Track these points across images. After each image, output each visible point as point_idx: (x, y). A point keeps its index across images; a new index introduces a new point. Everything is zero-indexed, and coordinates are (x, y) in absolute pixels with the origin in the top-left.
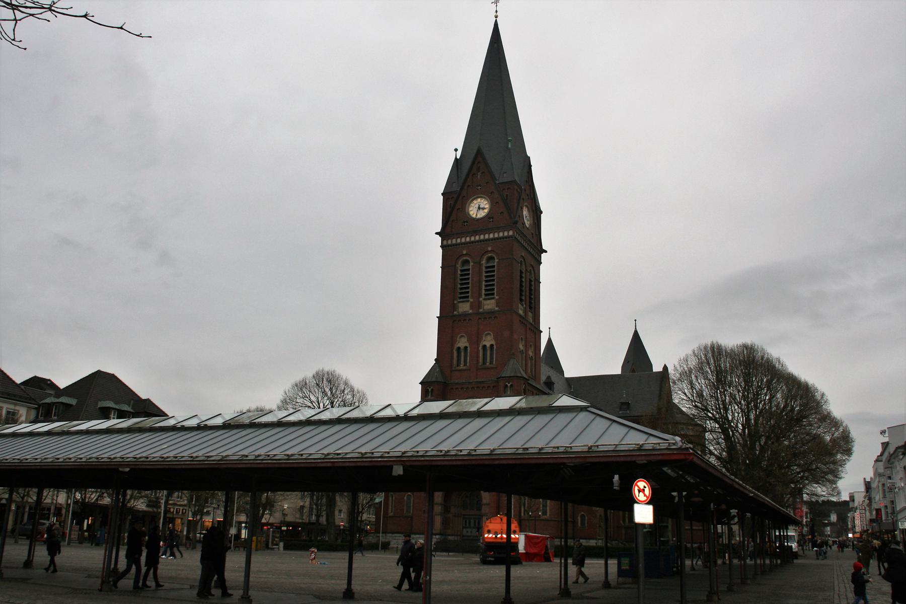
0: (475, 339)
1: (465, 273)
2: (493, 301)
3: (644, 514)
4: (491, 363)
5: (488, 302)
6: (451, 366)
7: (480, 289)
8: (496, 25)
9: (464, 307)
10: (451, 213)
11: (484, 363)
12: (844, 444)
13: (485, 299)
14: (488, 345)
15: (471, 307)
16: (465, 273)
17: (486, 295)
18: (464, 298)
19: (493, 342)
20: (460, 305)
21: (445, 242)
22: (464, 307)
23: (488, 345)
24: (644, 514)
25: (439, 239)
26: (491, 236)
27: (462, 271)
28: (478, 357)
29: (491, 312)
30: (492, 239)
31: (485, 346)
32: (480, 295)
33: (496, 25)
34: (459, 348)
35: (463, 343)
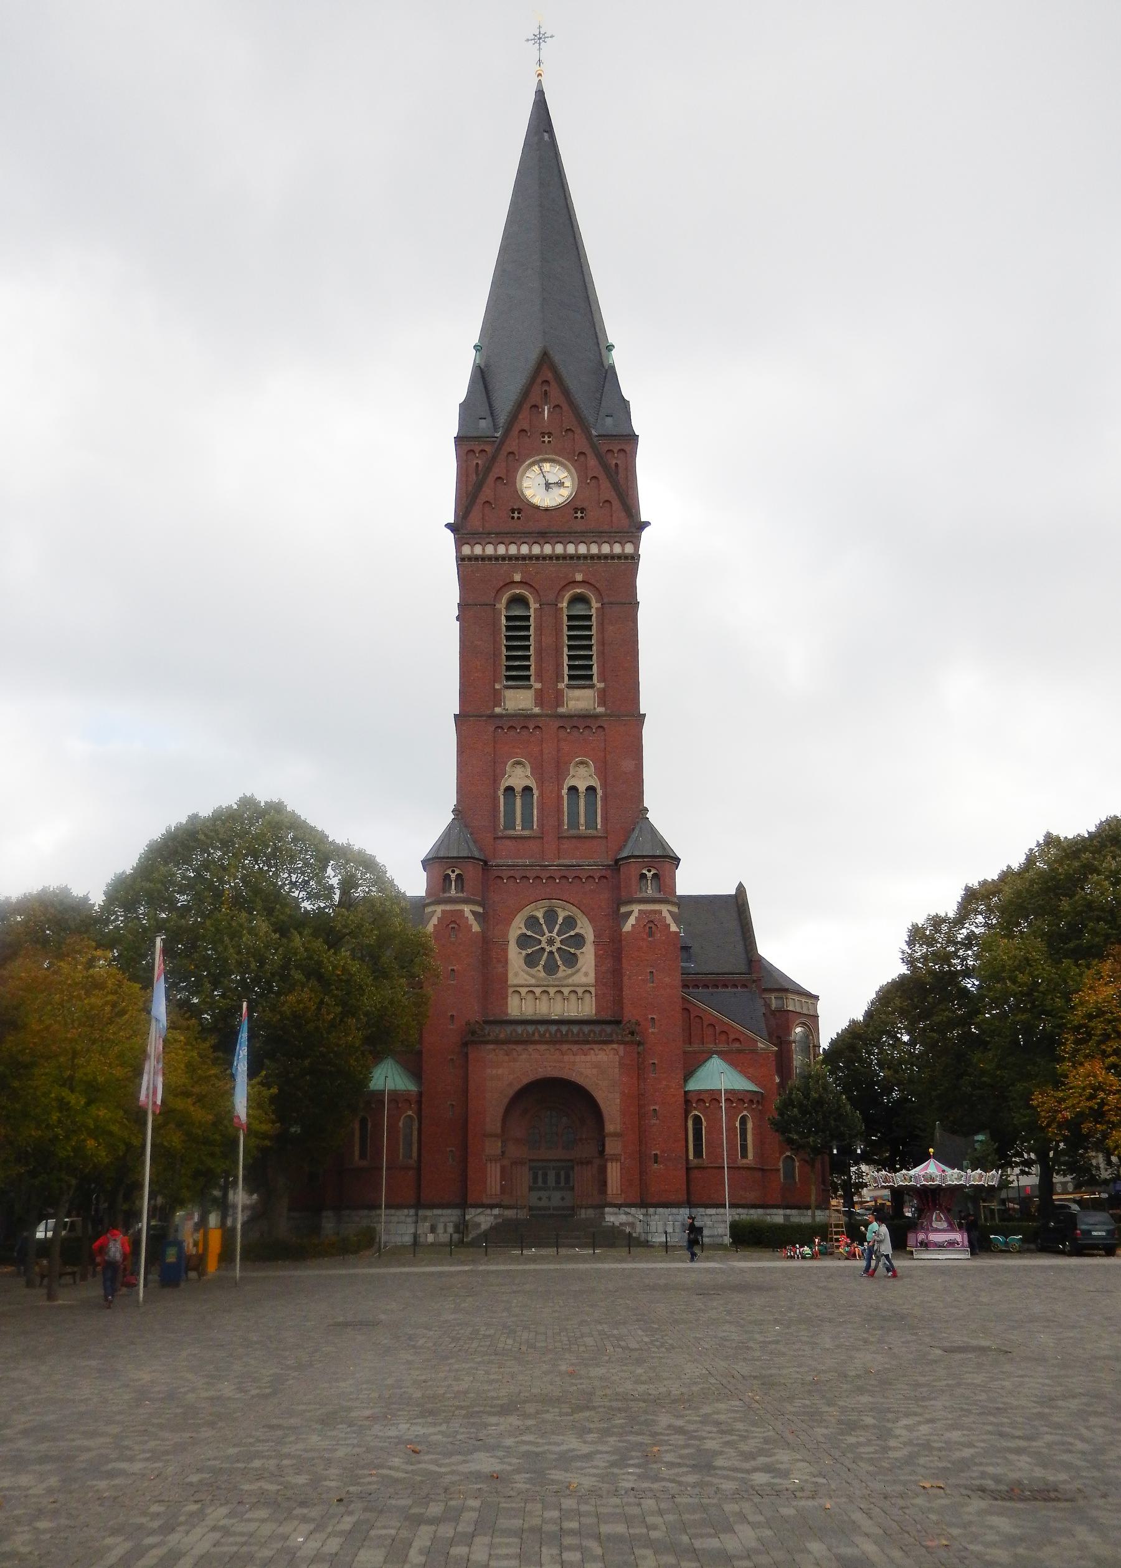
0: (550, 771)
1: (518, 624)
2: (588, 692)
3: (835, 1151)
4: (527, 821)
5: (577, 693)
6: (495, 827)
7: (559, 665)
8: (540, 94)
9: (519, 700)
10: (479, 486)
11: (510, 824)
12: (146, 1113)
13: (569, 687)
14: (582, 788)
15: (540, 698)
16: (518, 624)
17: (571, 677)
18: (518, 677)
19: (595, 782)
20: (509, 693)
21: (466, 550)
22: (519, 700)
23: (582, 788)
24: (835, 1151)
25: (450, 536)
26: (594, 549)
27: (508, 618)
28: (559, 810)
29: (585, 719)
30: (585, 557)
31: (573, 789)
32: (559, 677)
33: (540, 94)
34: (510, 789)
35: (518, 777)
